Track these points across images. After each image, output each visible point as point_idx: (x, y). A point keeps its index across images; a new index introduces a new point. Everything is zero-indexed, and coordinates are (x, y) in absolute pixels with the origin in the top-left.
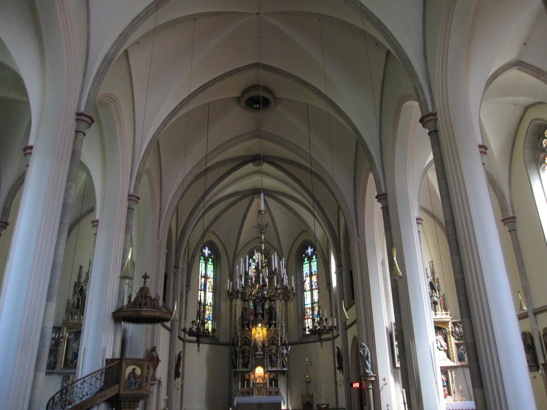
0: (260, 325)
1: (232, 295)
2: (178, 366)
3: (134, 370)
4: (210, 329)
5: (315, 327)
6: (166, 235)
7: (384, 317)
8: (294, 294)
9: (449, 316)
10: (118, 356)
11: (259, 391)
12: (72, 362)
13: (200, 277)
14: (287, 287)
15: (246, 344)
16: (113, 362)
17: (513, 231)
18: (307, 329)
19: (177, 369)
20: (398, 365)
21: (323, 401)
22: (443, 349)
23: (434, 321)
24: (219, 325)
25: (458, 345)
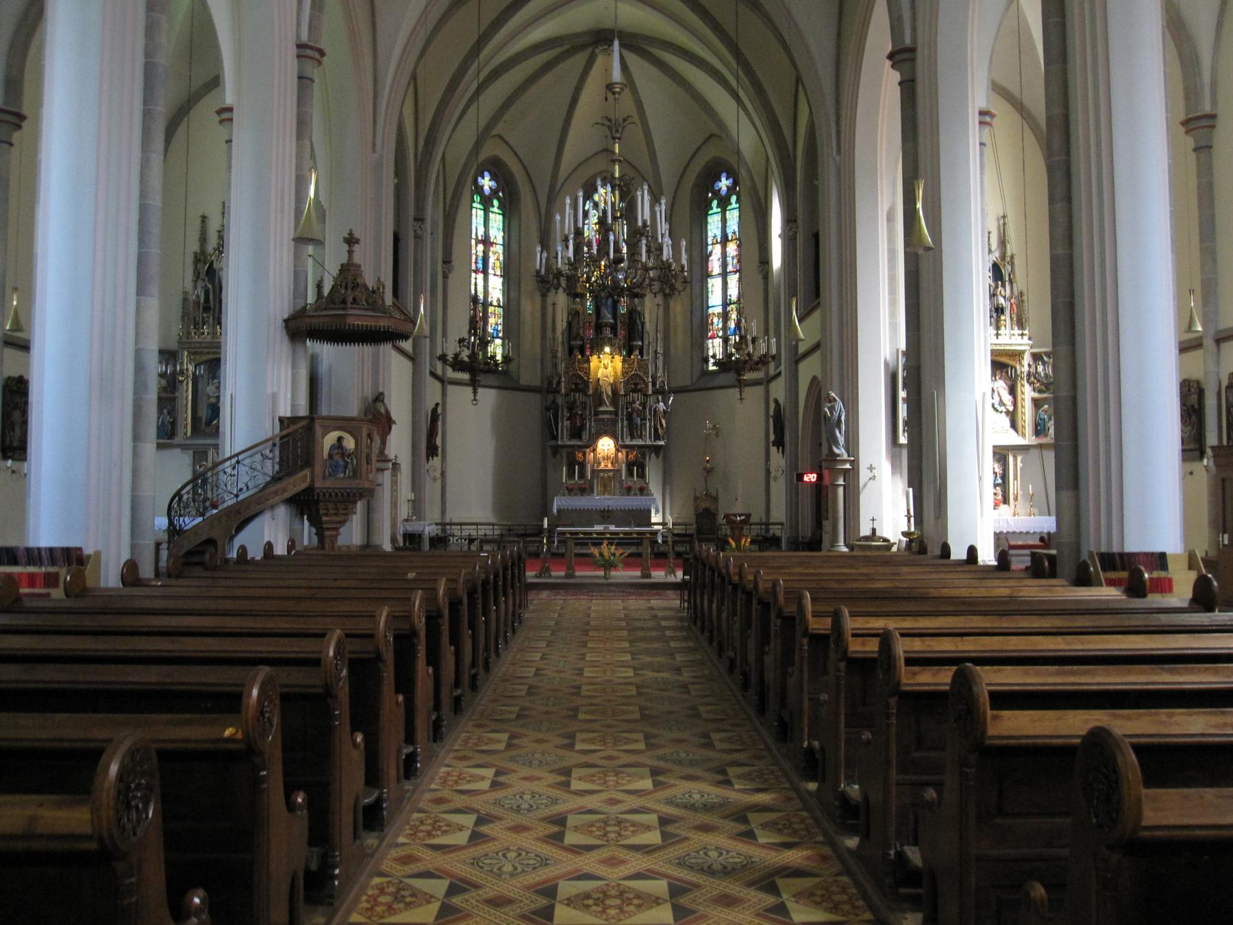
0: (607, 349)
1: (547, 282)
2: (432, 433)
3: (340, 439)
4: (499, 358)
5: (728, 356)
6: (393, 146)
7: (882, 335)
8: (685, 282)
9: (1026, 340)
10: (303, 411)
11: (605, 487)
12: (209, 423)
13: (473, 242)
14: (670, 265)
15: (577, 390)
16: (294, 424)
17: (1204, 149)
18: (712, 361)
19: (430, 441)
20: (903, 440)
21: (738, 508)
22: (1003, 409)
23: (992, 351)
24: (517, 347)
25: (1037, 403)
